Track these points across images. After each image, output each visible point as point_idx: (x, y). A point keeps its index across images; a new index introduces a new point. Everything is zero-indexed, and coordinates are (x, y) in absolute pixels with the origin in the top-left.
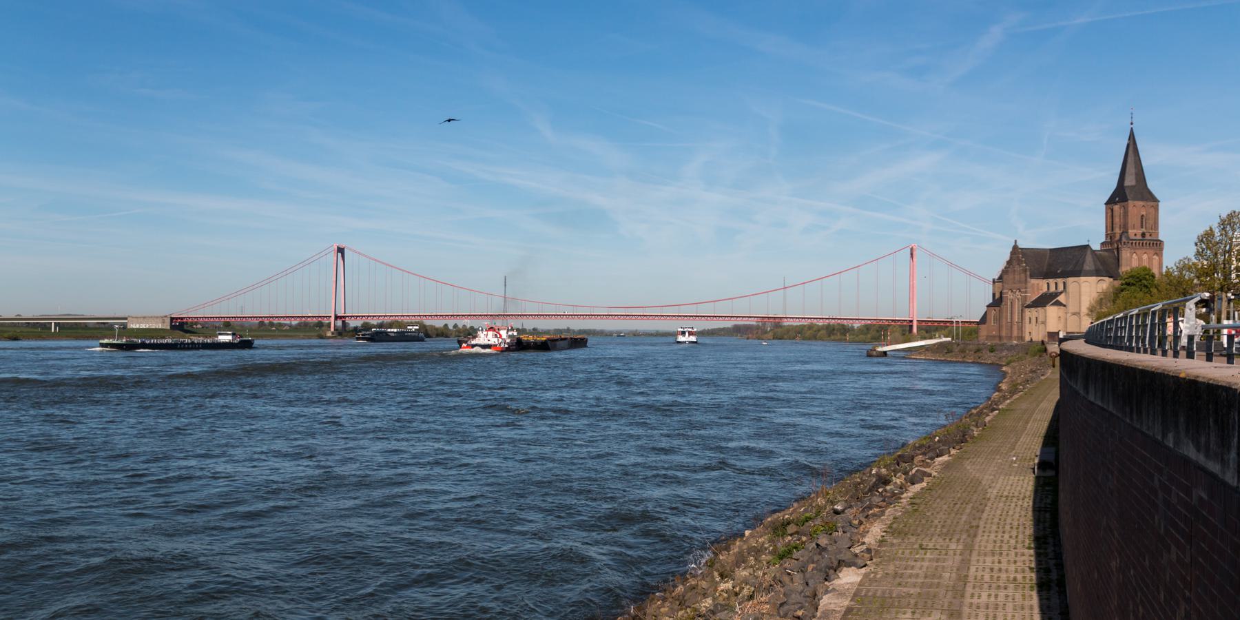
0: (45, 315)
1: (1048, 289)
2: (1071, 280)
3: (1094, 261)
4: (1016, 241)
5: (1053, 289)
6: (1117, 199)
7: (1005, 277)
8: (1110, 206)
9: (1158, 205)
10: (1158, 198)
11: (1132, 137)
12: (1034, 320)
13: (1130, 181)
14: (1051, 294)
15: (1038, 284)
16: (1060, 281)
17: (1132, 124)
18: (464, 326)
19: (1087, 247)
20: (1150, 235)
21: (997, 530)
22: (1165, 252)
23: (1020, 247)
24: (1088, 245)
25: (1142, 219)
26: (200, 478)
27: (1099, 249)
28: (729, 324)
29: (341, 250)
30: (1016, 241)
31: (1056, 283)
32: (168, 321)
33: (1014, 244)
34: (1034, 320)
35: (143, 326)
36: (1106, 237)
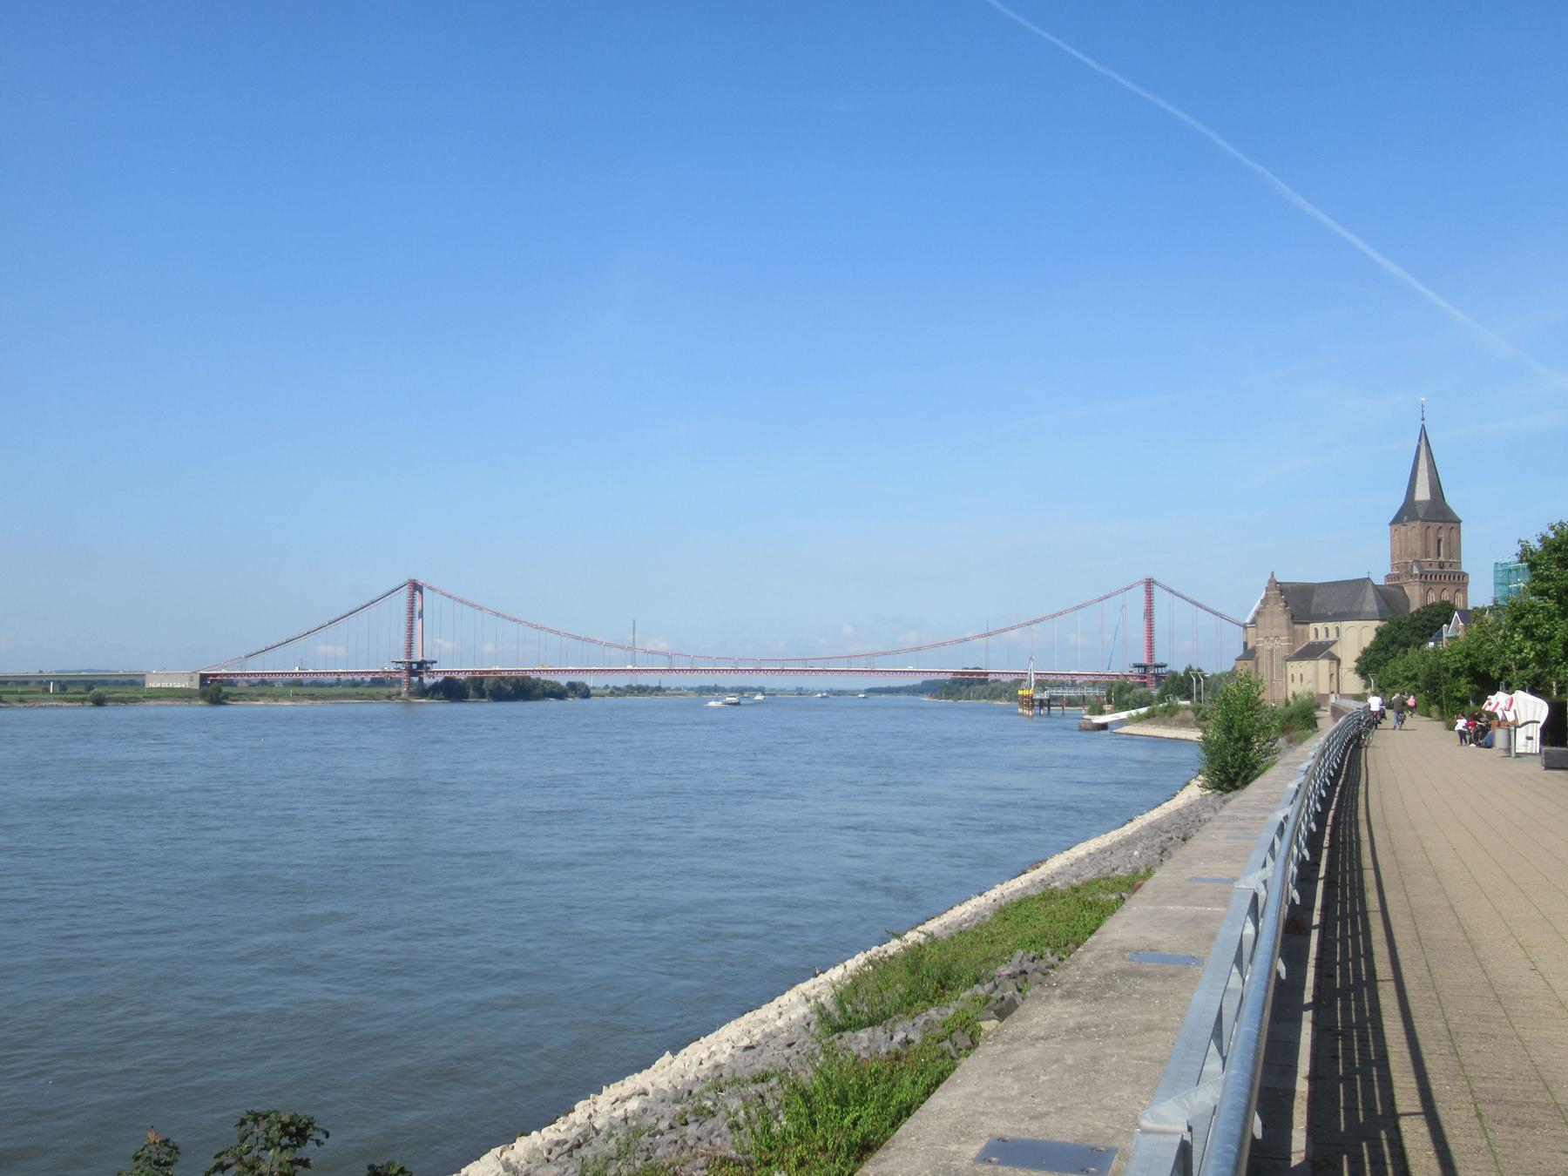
0: (64, 672)
1: (1327, 636)
2: (1346, 624)
3: (1375, 594)
4: (1272, 574)
5: (1322, 638)
6: (1405, 518)
7: (1260, 621)
8: (1396, 526)
9: (1460, 526)
10: (1459, 513)
11: (1423, 432)
12: (1297, 678)
13: (1423, 493)
14: (1320, 643)
15: (1303, 630)
16: (1331, 625)
17: (1423, 419)
18: (1310, 693)
19: (1363, 583)
20: (1451, 566)
21: (723, 1138)
22: (1470, 588)
23: (1278, 581)
24: (1368, 579)
25: (1439, 543)
26: (745, 826)
27: (1383, 584)
28: (917, 680)
29: (416, 587)
30: (1272, 574)
31: (1327, 629)
32: (197, 679)
33: (1270, 577)
34: (1297, 678)
35: (165, 685)
36: (1392, 568)
